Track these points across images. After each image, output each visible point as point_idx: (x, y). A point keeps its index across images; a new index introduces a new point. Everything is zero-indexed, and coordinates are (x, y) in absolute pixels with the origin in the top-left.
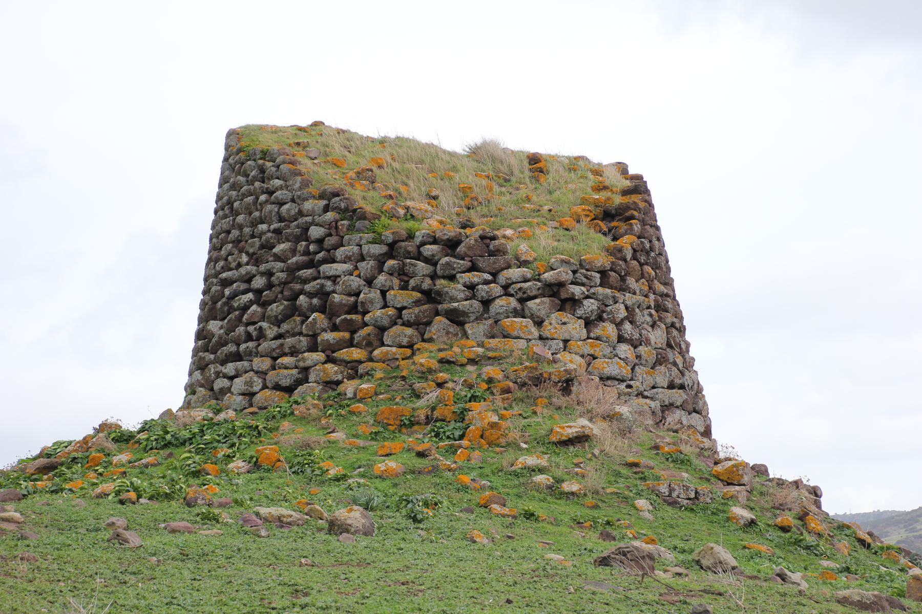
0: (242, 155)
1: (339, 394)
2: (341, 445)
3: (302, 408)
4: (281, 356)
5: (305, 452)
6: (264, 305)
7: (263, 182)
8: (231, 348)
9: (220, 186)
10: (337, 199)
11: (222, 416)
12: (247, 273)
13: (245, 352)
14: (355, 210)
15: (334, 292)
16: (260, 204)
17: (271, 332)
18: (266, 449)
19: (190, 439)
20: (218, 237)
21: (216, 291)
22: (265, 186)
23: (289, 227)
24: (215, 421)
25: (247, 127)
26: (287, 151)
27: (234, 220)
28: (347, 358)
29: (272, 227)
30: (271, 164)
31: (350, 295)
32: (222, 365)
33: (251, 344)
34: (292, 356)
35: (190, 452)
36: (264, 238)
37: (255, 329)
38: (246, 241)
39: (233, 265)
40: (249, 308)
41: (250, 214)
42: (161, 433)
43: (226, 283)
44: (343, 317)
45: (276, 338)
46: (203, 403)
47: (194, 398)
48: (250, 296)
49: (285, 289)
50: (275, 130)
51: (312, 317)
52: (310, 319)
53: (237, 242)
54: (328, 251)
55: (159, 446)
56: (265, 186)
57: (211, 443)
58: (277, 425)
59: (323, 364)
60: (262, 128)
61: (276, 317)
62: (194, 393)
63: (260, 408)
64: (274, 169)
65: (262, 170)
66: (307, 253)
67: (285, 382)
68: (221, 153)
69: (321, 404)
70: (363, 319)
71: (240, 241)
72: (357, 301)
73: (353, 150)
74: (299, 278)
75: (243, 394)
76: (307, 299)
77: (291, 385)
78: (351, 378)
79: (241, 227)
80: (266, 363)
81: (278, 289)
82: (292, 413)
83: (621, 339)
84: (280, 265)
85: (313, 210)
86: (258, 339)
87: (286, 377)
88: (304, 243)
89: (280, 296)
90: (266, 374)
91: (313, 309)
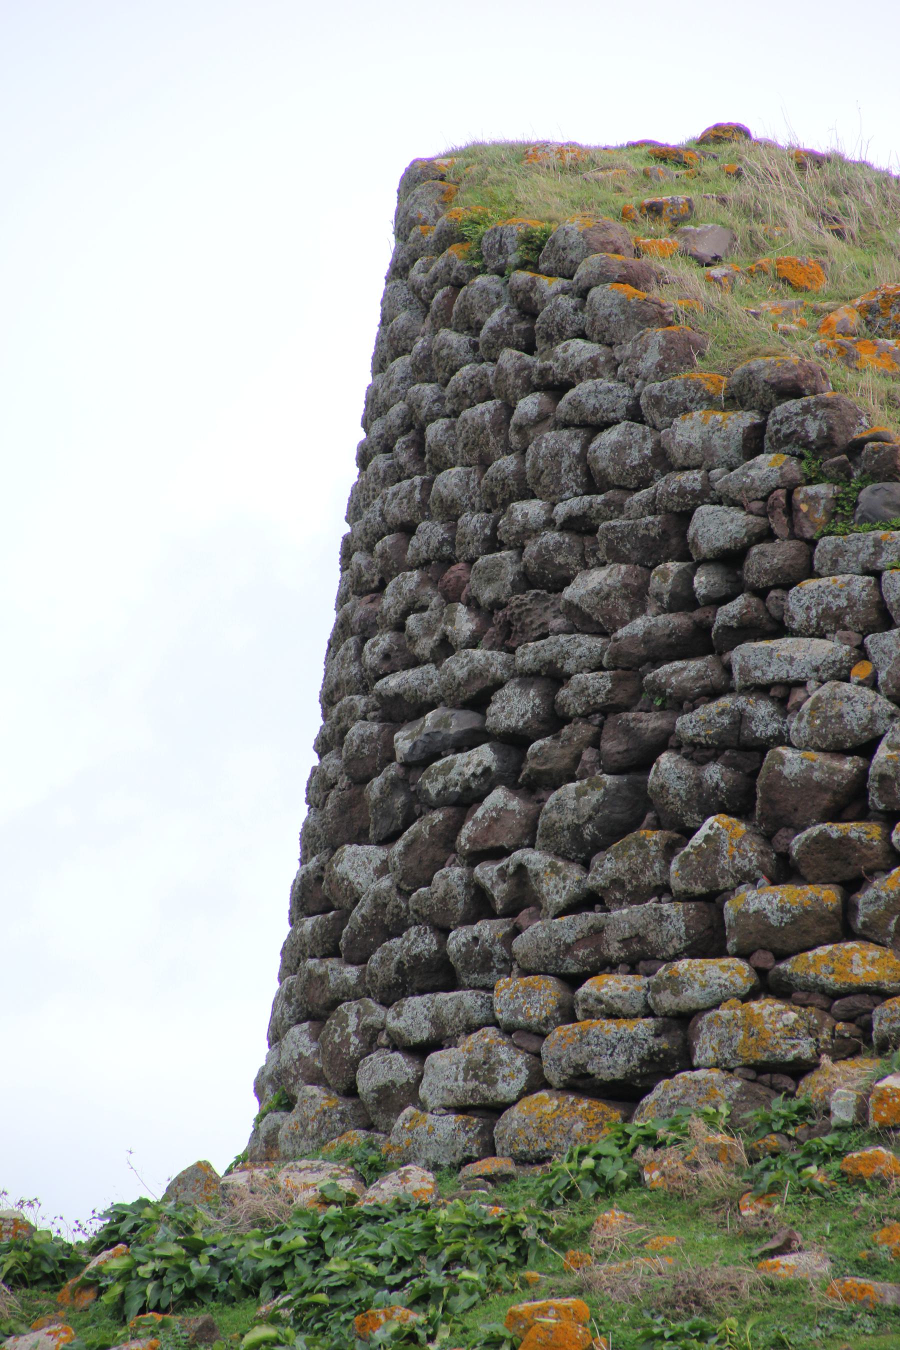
0: (455, 252)
1: (803, 1111)
2: (816, 1299)
3: (671, 1159)
4: (594, 972)
5: (686, 1325)
6: (534, 787)
7: (530, 349)
8: (418, 942)
9: (380, 365)
10: (793, 405)
11: (386, 1190)
12: (473, 675)
13: (467, 957)
14: (856, 448)
15: (781, 739)
16: (520, 429)
17: (558, 883)
18: (543, 1312)
19: (277, 1272)
20: (370, 549)
21: (363, 740)
22: (536, 362)
23: (620, 508)
24: (362, 1206)
25: (473, 153)
26: (614, 236)
27: (427, 485)
28: (831, 981)
29: (561, 510)
30: (558, 283)
31: (839, 751)
32: (386, 1004)
33: (487, 929)
34: (633, 970)
35: (274, 1320)
36: (531, 548)
37: (502, 873)
38: (471, 561)
39: (425, 646)
40: (480, 800)
41: (485, 463)
42: (173, 1250)
43: (399, 711)
44: (814, 831)
45: (575, 907)
46: (319, 1139)
47: (288, 1121)
48: (484, 755)
49: (608, 731)
50: (575, 162)
51: (704, 830)
52: (697, 839)
53: (437, 564)
54: (761, 593)
55: (167, 1299)
56: (536, 362)
57: (351, 1285)
58: (580, 1222)
59: (745, 999)
60: (526, 156)
61: (576, 830)
62: (287, 1104)
63: (522, 1160)
64: (568, 303)
65: (527, 308)
66: (684, 600)
67: (611, 1067)
68: (383, 248)
69: (739, 1145)
70: (887, 838)
71: (450, 561)
72: (864, 774)
73: (852, 226)
74: (658, 690)
75: (461, 1110)
76: (685, 768)
77: (630, 1077)
78: (846, 1051)
79: (450, 513)
80: (537, 998)
81: (582, 731)
82: (636, 1179)
84: (588, 645)
85: (707, 449)
86: (511, 911)
87: (614, 1046)
88: (673, 567)
89: (588, 755)
90: (543, 1036)
91: (708, 803)
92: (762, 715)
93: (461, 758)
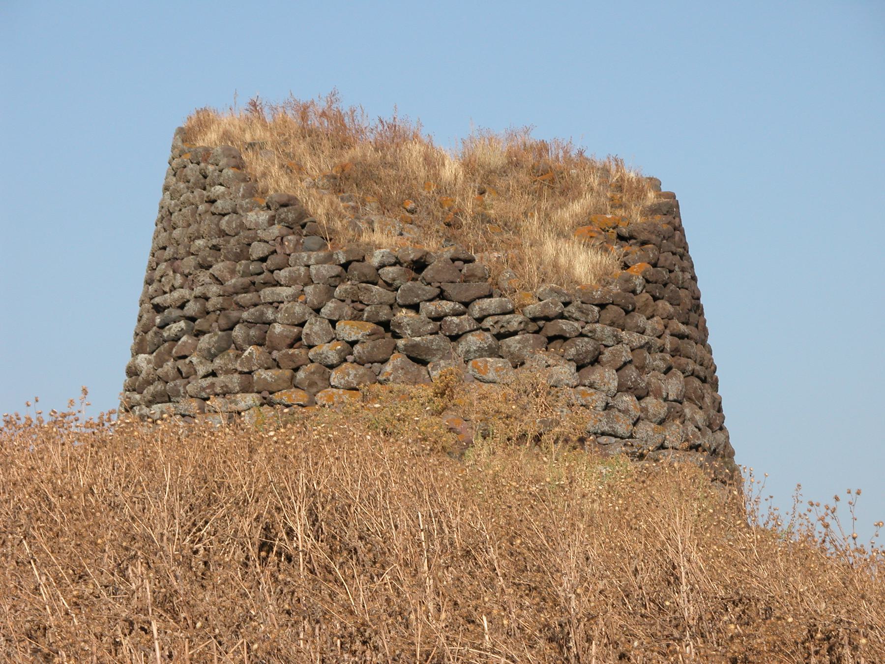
6: (199, 334)
8: (159, 386)
27: (171, 233)
40: (179, 339)
43: (158, 309)
51: (249, 350)
52: (246, 353)
61: (209, 350)
92: (270, 314)
93: (174, 325)
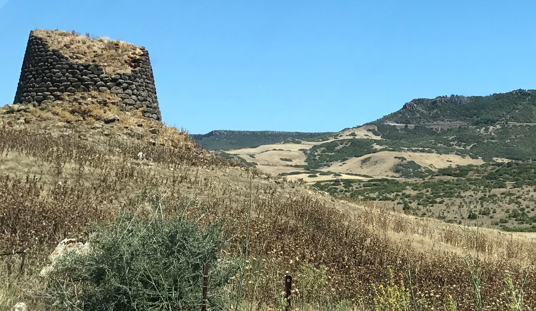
43: (26, 72)
83: (133, 94)
